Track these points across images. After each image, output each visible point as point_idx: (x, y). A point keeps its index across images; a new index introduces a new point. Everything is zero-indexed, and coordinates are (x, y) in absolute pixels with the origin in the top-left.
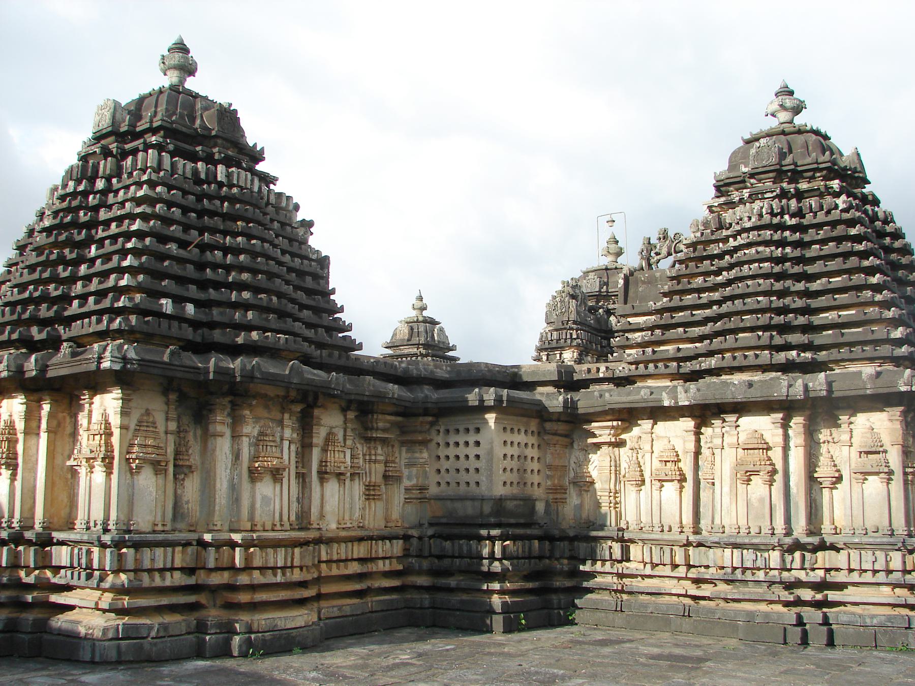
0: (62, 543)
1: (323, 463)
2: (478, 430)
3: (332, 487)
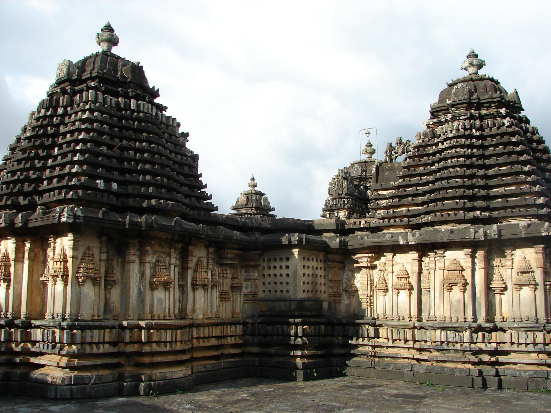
1: (194, 279)
3: (200, 293)
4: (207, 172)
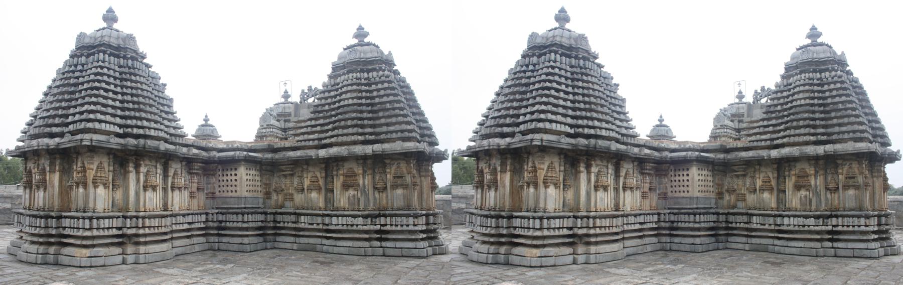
0: (66, 217)
1: (173, 183)
2: (236, 169)
3: (177, 192)
4: (631, 109)
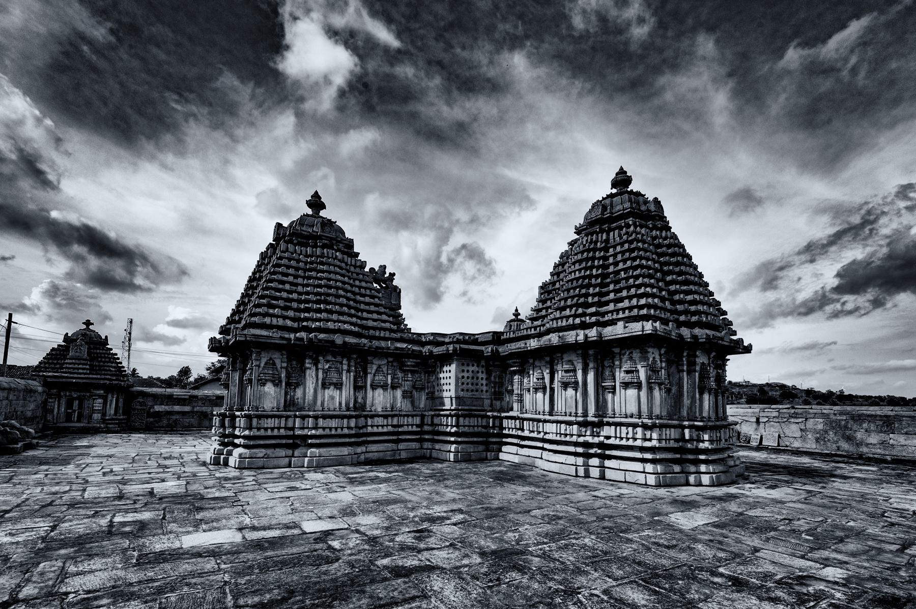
1: (372, 382)
3: (379, 391)
